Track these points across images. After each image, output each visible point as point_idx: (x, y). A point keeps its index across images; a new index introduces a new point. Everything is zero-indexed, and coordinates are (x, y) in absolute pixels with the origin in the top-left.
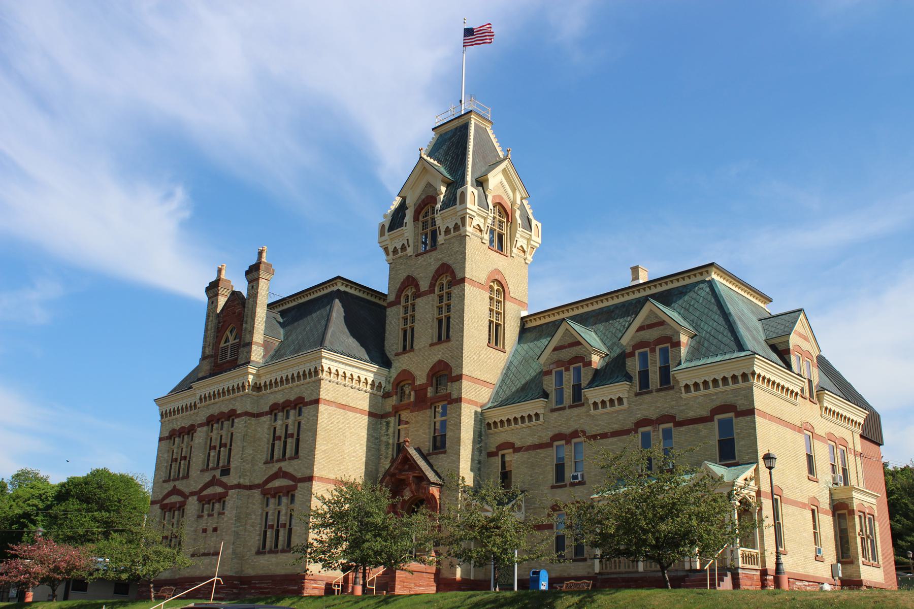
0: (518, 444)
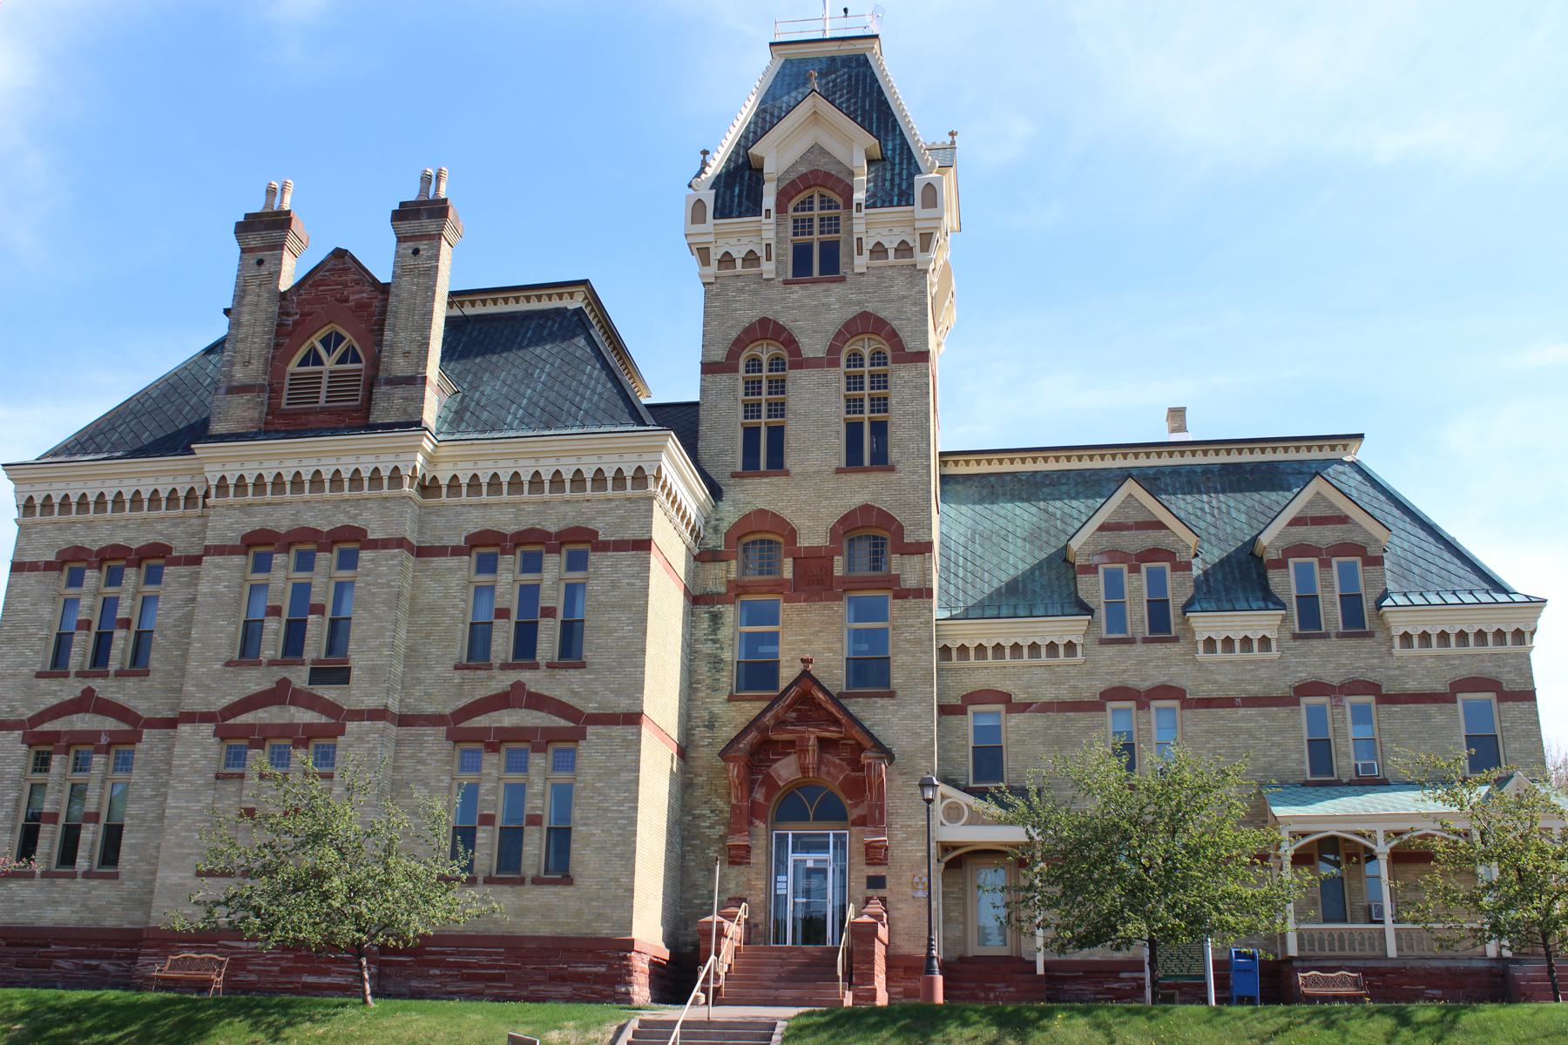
0: (1019, 696)
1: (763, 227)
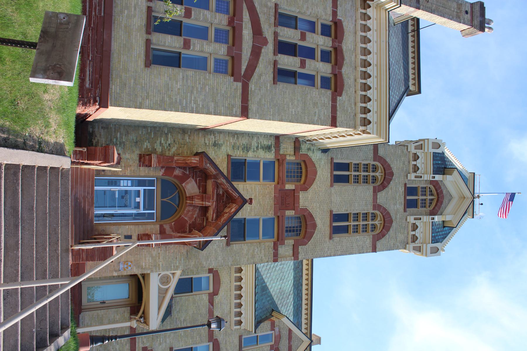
0: (217, 299)
1: (429, 175)
